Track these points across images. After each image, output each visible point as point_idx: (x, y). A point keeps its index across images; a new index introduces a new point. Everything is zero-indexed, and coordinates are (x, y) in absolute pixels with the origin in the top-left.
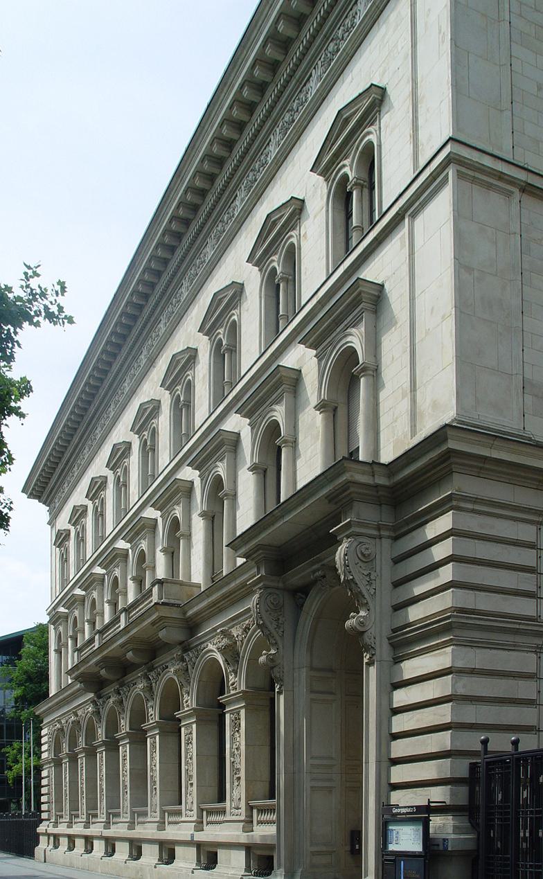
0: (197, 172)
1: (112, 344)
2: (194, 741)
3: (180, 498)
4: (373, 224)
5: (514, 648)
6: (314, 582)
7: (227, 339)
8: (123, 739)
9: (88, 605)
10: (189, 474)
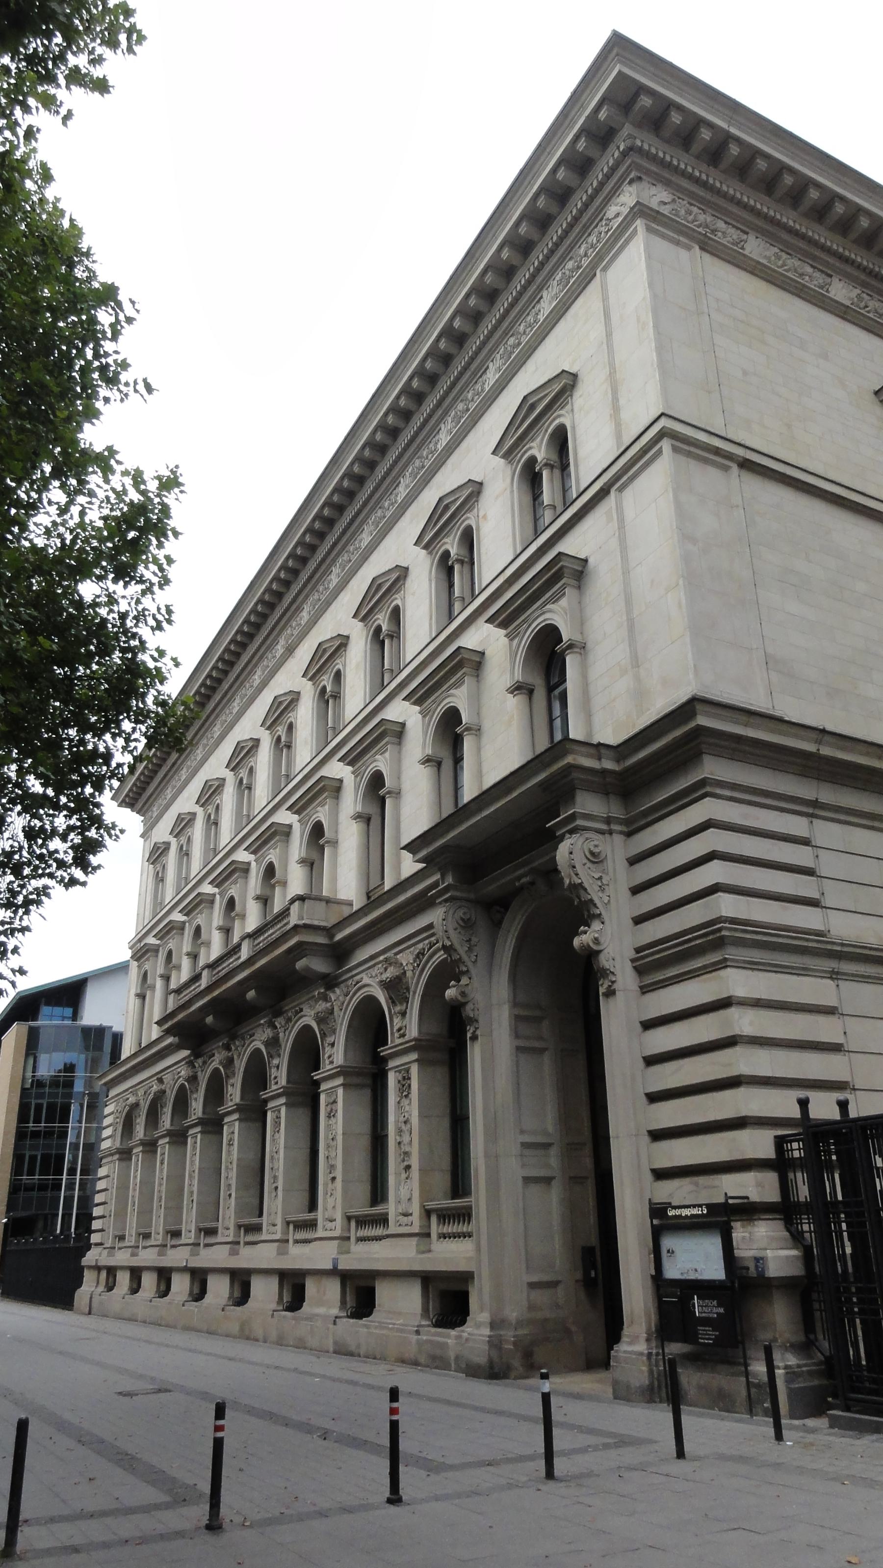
0: (357, 459)
1: (258, 614)
2: (236, 1143)
3: (325, 799)
4: (474, 597)
5: (803, 972)
6: (522, 888)
7: (388, 624)
8: (229, 1113)
9: (189, 932)
10: (337, 769)
